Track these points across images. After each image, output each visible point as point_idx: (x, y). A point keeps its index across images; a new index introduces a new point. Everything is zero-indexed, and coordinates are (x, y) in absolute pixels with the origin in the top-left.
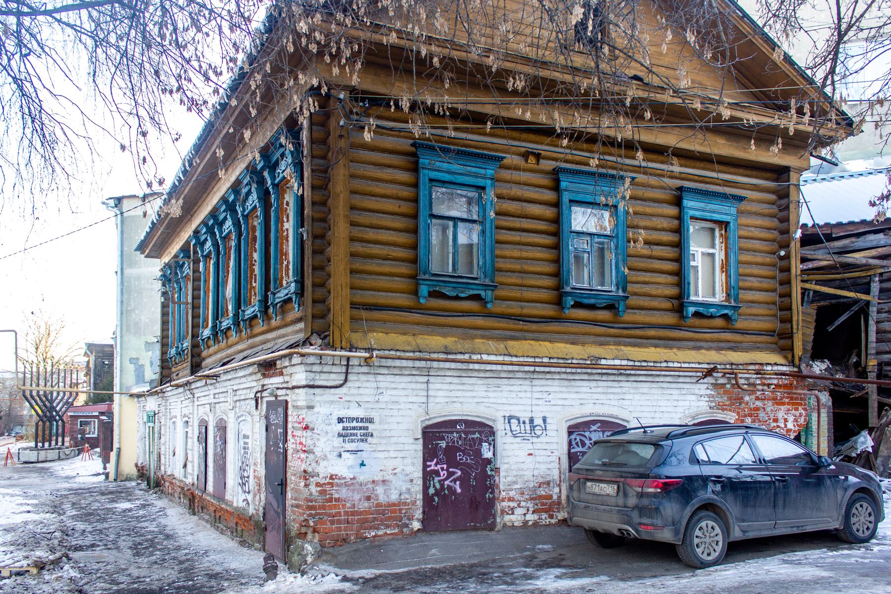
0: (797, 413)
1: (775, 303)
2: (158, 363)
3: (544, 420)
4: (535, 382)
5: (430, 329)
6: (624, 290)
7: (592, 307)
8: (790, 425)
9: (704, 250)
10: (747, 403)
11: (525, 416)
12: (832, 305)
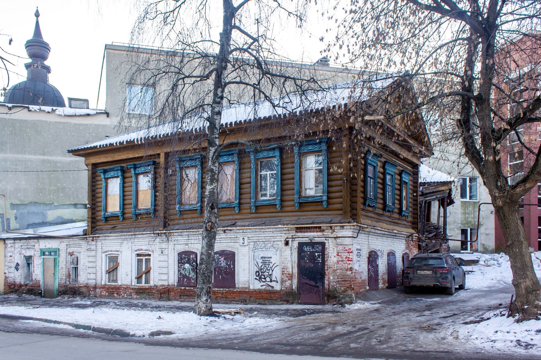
11: (381, 249)
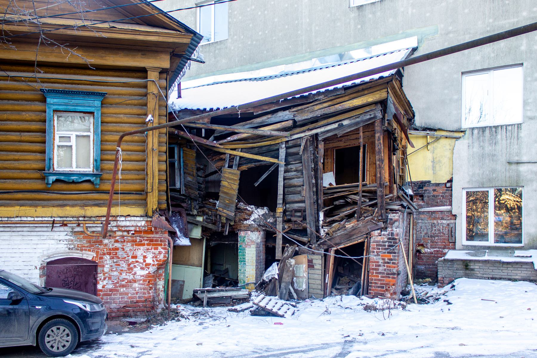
0: (157, 252)
8: (149, 260)
10: (106, 245)
12: (250, 169)
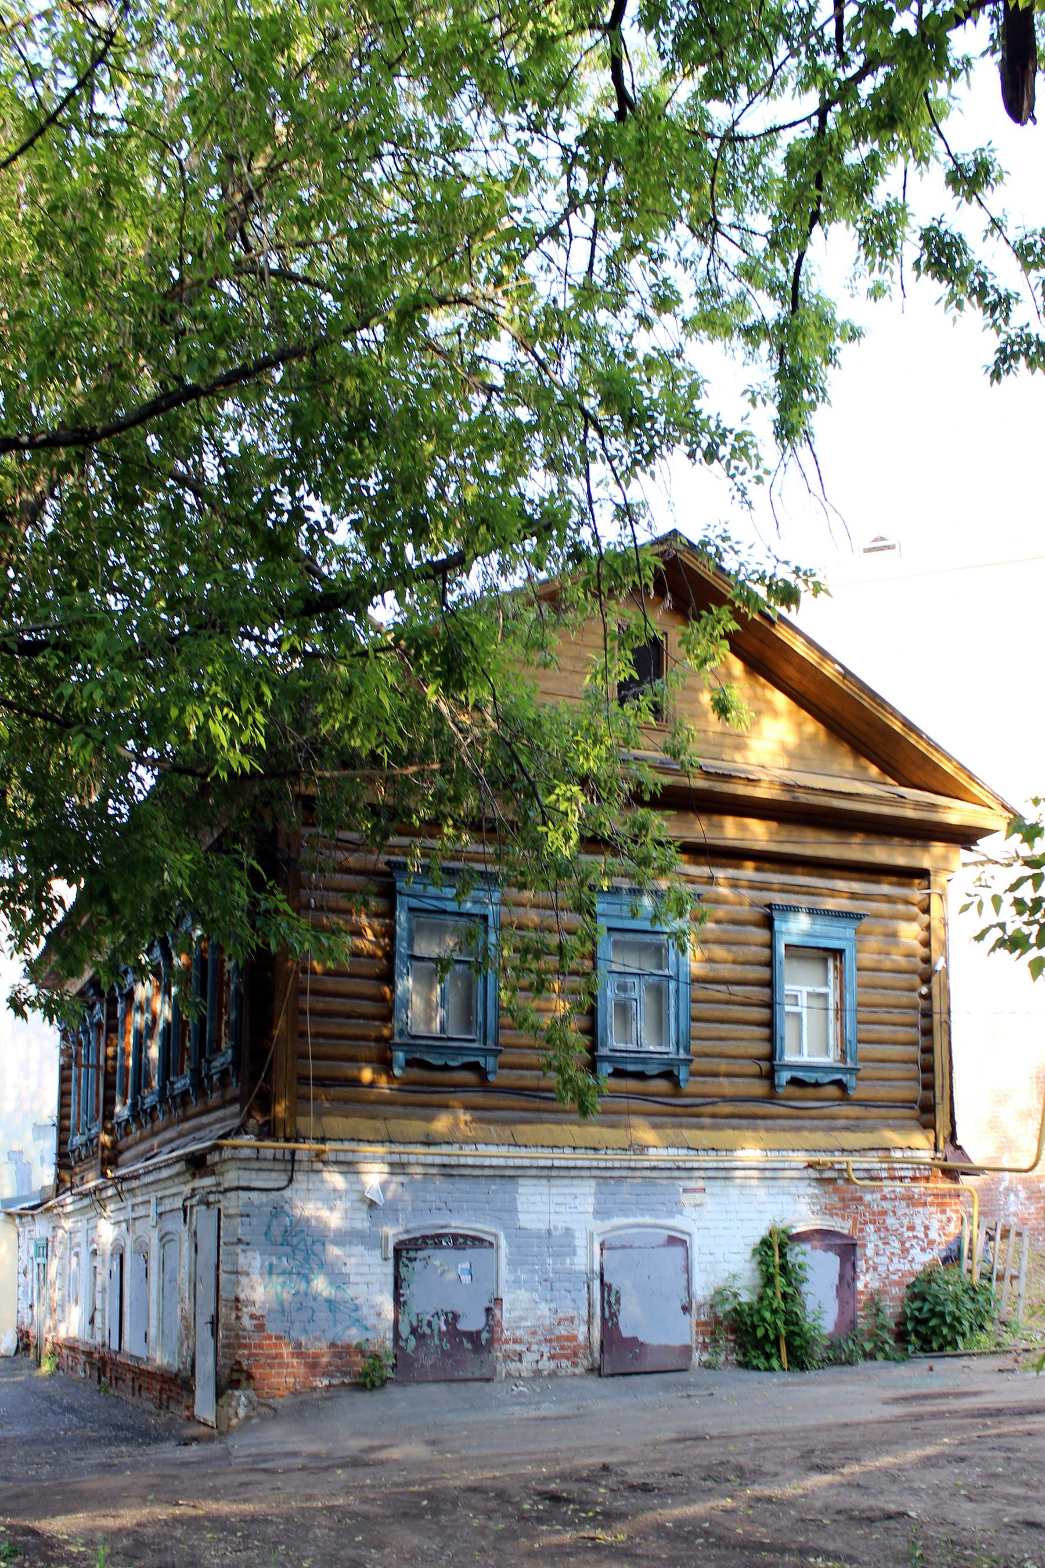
1: (915, 1062)
2: (53, 1158)
3: (979, 938)
4: (554, 1182)
5: (409, 1110)
6: (687, 1050)
7: (641, 1076)
9: (810, 989)
10: (868, 1205)
